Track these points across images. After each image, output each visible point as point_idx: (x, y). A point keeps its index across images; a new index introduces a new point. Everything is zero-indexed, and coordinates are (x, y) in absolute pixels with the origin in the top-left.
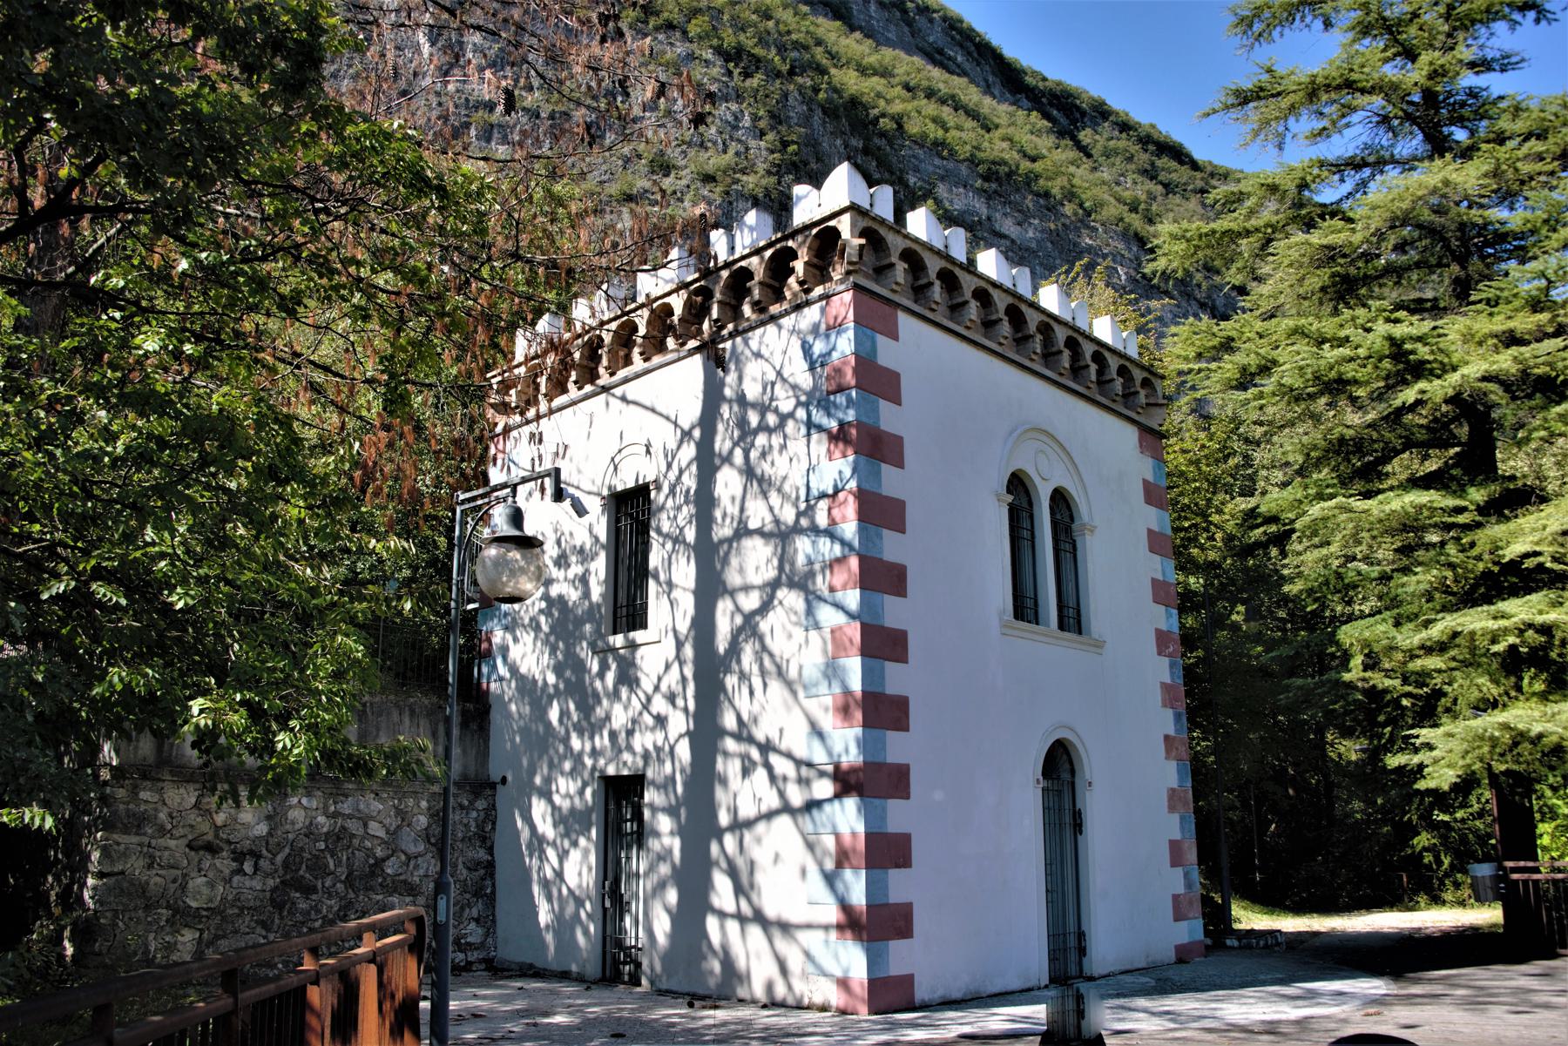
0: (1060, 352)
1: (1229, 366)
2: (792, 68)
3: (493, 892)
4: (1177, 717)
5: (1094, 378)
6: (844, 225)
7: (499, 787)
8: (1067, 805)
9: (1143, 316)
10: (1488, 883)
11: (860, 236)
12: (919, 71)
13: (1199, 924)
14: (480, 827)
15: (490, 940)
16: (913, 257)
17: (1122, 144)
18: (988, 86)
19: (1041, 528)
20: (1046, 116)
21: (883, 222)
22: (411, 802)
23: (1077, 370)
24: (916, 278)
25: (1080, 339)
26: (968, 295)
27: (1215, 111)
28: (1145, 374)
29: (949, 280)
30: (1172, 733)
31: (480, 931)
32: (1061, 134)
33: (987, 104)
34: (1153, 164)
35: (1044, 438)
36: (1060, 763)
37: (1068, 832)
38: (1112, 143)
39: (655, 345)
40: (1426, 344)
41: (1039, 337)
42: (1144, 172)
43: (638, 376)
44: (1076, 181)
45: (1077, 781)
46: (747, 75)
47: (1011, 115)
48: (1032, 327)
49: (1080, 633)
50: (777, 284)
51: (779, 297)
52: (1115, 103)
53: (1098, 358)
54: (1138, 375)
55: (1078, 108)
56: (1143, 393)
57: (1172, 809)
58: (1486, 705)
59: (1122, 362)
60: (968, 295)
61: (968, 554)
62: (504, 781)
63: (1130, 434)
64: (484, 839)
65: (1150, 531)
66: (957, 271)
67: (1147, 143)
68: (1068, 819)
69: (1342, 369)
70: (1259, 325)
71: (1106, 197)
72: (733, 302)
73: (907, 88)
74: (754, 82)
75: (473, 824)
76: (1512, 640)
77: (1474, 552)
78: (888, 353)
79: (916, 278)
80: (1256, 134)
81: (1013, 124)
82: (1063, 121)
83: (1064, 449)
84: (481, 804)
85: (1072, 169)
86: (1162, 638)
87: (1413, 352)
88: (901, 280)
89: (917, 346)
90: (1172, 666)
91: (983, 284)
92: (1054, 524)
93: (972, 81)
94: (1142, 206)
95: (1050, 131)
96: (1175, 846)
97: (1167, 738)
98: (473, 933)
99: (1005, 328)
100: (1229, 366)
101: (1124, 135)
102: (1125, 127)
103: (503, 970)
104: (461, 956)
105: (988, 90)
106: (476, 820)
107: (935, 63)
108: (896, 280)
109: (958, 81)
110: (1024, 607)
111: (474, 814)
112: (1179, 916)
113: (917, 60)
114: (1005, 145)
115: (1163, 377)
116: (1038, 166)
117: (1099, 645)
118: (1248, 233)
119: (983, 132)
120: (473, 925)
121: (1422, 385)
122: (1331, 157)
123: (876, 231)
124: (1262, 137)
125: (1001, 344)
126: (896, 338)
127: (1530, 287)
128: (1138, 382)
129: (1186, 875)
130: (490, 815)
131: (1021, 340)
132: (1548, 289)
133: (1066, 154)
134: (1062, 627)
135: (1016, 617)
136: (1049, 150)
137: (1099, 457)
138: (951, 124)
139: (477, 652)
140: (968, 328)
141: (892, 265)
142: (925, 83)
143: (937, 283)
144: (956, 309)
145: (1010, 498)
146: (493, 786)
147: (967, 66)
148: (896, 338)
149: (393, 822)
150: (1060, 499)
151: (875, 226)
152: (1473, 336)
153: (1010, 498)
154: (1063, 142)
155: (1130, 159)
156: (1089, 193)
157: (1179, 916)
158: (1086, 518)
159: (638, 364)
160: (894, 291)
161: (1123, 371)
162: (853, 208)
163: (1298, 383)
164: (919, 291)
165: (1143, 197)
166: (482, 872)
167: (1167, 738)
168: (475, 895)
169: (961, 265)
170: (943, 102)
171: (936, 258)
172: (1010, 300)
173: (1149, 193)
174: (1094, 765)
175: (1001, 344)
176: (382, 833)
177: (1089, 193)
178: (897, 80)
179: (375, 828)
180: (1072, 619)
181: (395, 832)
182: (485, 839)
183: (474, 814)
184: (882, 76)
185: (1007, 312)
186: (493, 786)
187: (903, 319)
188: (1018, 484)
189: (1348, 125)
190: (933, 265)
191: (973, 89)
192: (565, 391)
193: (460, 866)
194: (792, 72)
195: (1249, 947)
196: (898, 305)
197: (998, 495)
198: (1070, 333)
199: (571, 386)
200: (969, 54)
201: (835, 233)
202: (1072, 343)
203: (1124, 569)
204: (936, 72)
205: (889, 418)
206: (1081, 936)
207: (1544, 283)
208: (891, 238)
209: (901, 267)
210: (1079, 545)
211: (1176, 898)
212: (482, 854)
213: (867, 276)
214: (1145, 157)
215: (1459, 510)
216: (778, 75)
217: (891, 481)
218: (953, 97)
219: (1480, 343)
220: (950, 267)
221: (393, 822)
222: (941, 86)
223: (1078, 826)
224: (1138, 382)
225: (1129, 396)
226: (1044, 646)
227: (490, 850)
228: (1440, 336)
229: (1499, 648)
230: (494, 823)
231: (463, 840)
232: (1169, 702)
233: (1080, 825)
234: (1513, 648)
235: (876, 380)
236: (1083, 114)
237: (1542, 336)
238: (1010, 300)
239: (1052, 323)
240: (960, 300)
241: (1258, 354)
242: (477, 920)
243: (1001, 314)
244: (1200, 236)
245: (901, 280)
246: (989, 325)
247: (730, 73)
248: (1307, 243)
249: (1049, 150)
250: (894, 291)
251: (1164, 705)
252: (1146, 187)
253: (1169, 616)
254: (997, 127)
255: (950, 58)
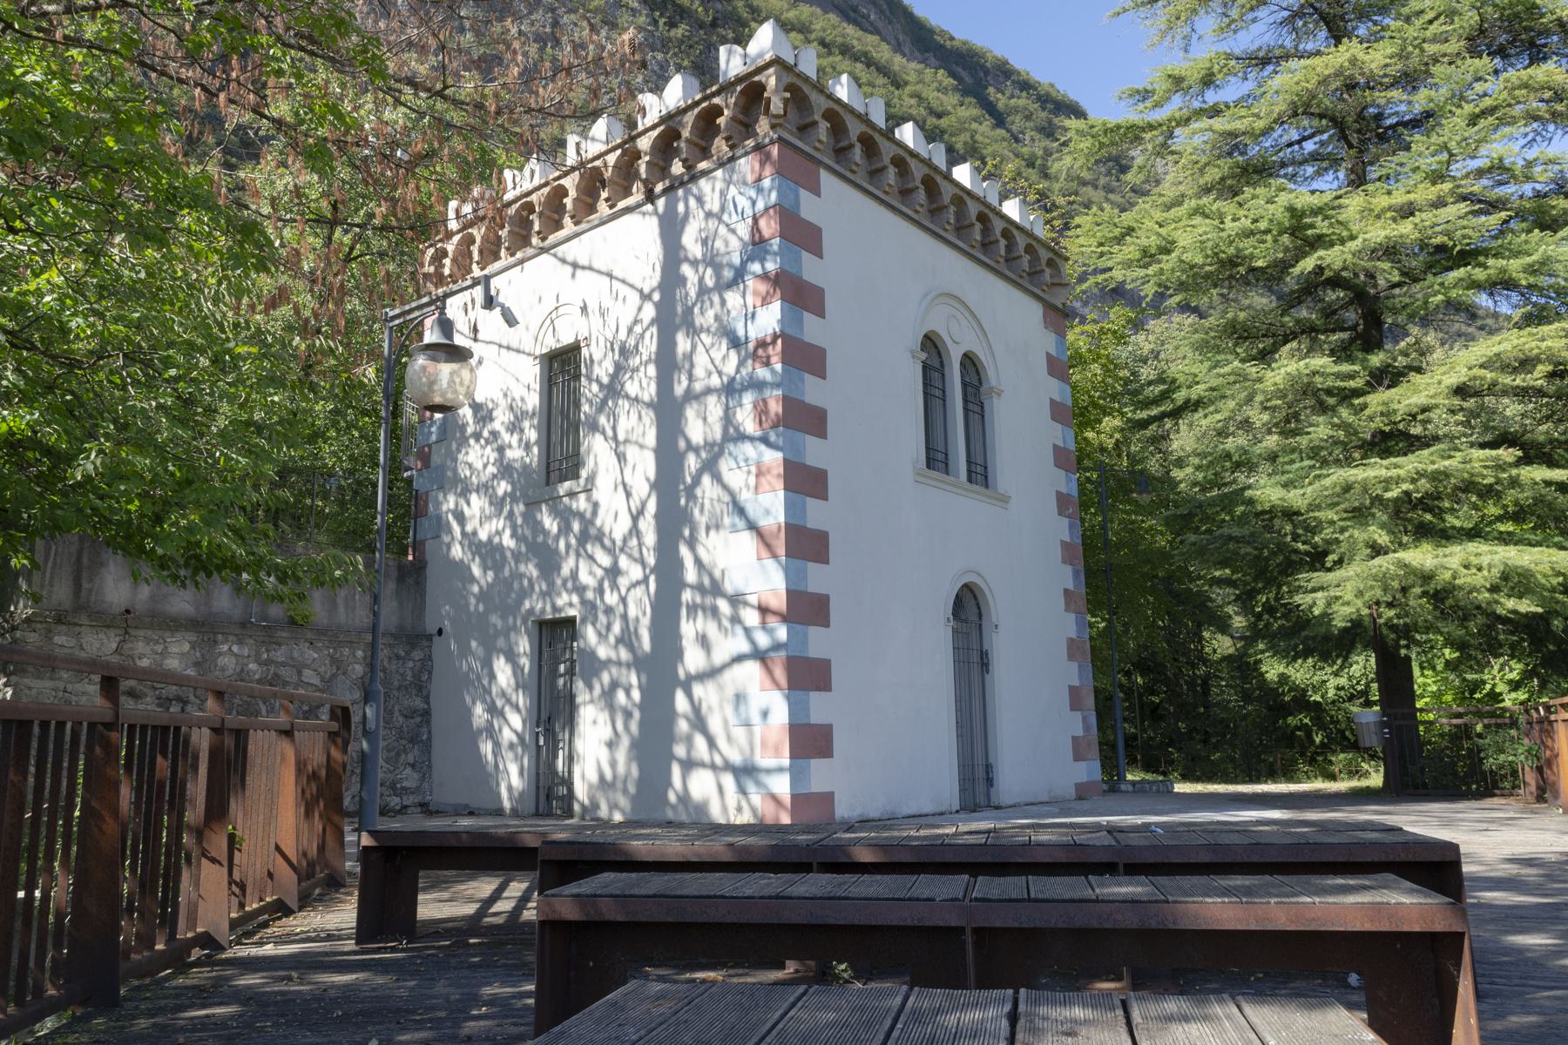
0: (973, 225)
1: (1130, 250)
2: (715, 19)
3: (429, 739)
4: (1076, 573)
5: (1003, 252)
6: (771, 80)
7: (436, 639)
8: (975, 646)
9: (1048, 211)
10: (1373, 728)
11: (786, 90)
12: (834, 27)
13: (1096, 765)
14: (417, 676)
15: (426, 785)
16: (837, 116)
17: (1022, 102)
18: (899, 45)
19: (952, 392)
20: (952, 74)
21: (806, 79)
22: (346, 651)
23: (987, 245)
24: (837, 141)
25: (991, 215)
26: (887, 161)
27: (1125, 10)
28: (1051, 255)
29: (869, 145)
30: (1071, 587)
31: (416, 776)
32: (966, 92)
33: (898, 62)
34: (1050, 122)
35: (952, 302)
36: (968, 607)
37: (976, 669)
38: (1013, 101)
39: (587, 205)
40: (1326, 217)
41: (952, 209)
42: (1041, 130)
43: (568, 239)
44: (978, 137)
45: (984, 623)
46: (672, 24)
47: (920, 72)
48: (946, 199)
49: (987, 486)
50: (703, 143)
51: (705, 153)
52: (1017, 63)
53: (1006, 234)
54: (1044, 255)
55: (983, 67)
56: (1048, 271)
57: (1071, 657)
58: (1377, 550)
59: (1030, 241)
60: (887, 161)
61: (877, 407)
62: (440, 632)
63: (1034, 310)
64: (420, 689)
65: (1052, 401)
66: (877, 137)
67: (1046, 101)
68: (975, 658)
69: (1241, 245)
70: (1158, 215)
71: (1006, 152)
72: (661, 163)
73: (823, 43)
74: (680, 31)
75: (409, 673)
76: (1405, 486)
77: (1367, 412)
78: (809, 208)
79: (837, 141)
80: (1164, 34)
81: (920, 81)
82: (968, 79)
83: (975, 316)
84: (417, 654)
85: (974, 126)
86: (1062, 500)
87: (1312, 226)
88: (823, 138)
89: (836, 204)
90: (1071, 526)
91: (901, 152)
92: (965, 385)
93: (883, 39)
94: (1039, 162)
95: (955, 89)
96: (1074, 692)
97: (1066, 591)
98: (409, 778)
99: (921, 195)
100: (1130, 250)
101: (1024, 94)
102: (1026, 86)
103: (437, 812)
104: (397, 800)
105: (898, 49)
106: (412, 669)
107: (850, 20)
108: (818, 139)
109: (872, 39)
110: (936, 458)
111: (411, 664)
112: (1078, 757)
113: (833, 18)
114: (913, 101)
115: (1067, 259)
116: (944, 122)
117: (1004, 499)
118: (1151, 127)
119: (892, 89)
120: (408, 771)
121: (1321, 253)
122: (1237, 52)
123: (800, 89)
124: (1169, 37)
125: (917, 212)
126: (818, 194)
127: (1429, 162)
128: (1043, 262)
129: (1084, 719)
130: (426, 665)
131: (936, 211)
132: (1448, 163)
133: (969, 110)
134: (970, 480)
135: (928, 466)
136: (954, 107)
137: (1005, 326)
138: (864, 80)
139: (411, 508)
140: (886, 193)
141: (815, 123)
142: (839, 40)
143: (858, 145)
144: (875, 174)
145: (924, 356)
146: (430, 637)
147: (880, 25)
148: (818, 194)
149: (327, 670)
150: (969, 361)
151: (799, 83)
152: (1371, 210)
153: (924, 356)
154: (968, 100)
155: (1028, 117)
156: (990, 149)
157: (1078, 757)
158: (993, 382)
159: (569, 226)
160: (817, 149)
161: (1029, 249)
162: (777, 62)
163: (1199, 260)
164: (841, 152)
165: (1041, 153)
166: (418, 719)
167: (1066, 591)
168: (411, 741)
169: (880, 131)
170: (856, 59)
171: (856, 121)
172: (926, 170)
173: (1046, 150)
174: (1002, 607)
175: (917, 212)
176: (316, 681)
177: (990, 149)
178: (813, 36)
179: (309, 676)
180: (980, 474)
181: (330, 680)
182: (420, 686)
183: (411, 664)
184: (800, 31)
185: (923, 182)
186: (430, 637)
187: (824, 175)
188: (931, 343)
189: (1254, 20)
190: (855, 129)
191: (885, 46)
192: (497, 257)
193: (397, 713)
194: (714, 24)
195: (1143, 791)
196: (820, 163)
197: (912, 352)
198: (982, 208)
199: (503, 253)
200: (882, 12)
201: (761, 87)
202: (982, 218)
203: (1025, 430)
204: (850, 30)
205: (811, 269)
206: (988, 768)
207: (1445, 156)
208: (814, 97)
209: (824, 126)
210: (986, 407)
211: (1075, 739)
212: (418, 703)
213: (792, 134)
214: (1044, 115)
215: (1351, 376)
216: (701, 26)
217: (813, 330)
218: (865, 54)
219: (1378, 217)
220: (870, 132)
221: (327, 670)
222: (855, 43)
223: (984, 664)
224: (1043, 262)
225: (1034, 274)
226: (954, 502)
227: (427, 699)
228: (1340, 207)
229: (1393, 493)
230: (430, 673)
231: (399, 689)
232: (1068, 559)
233: (987, 665)
234: (1407, 493)
235: (801, 234)
236: (987, 72)
237: (1439, 203)
238: (926, 170)
239: (965, 196)
240: (879, 165)
241: (1159, 235)
242: (413, 766)
243: (918, 183)
244: (1105, 132)
245: (823, 138)
246: (905, 193)
247: (655, 22)
248: (1211, 129)
249: (954, 107)
250: (817, 149)
251: (1064, 562)
252: (1043, 144)
253: (1069, 480)
254: (906, 83)
255: (863, 16)
